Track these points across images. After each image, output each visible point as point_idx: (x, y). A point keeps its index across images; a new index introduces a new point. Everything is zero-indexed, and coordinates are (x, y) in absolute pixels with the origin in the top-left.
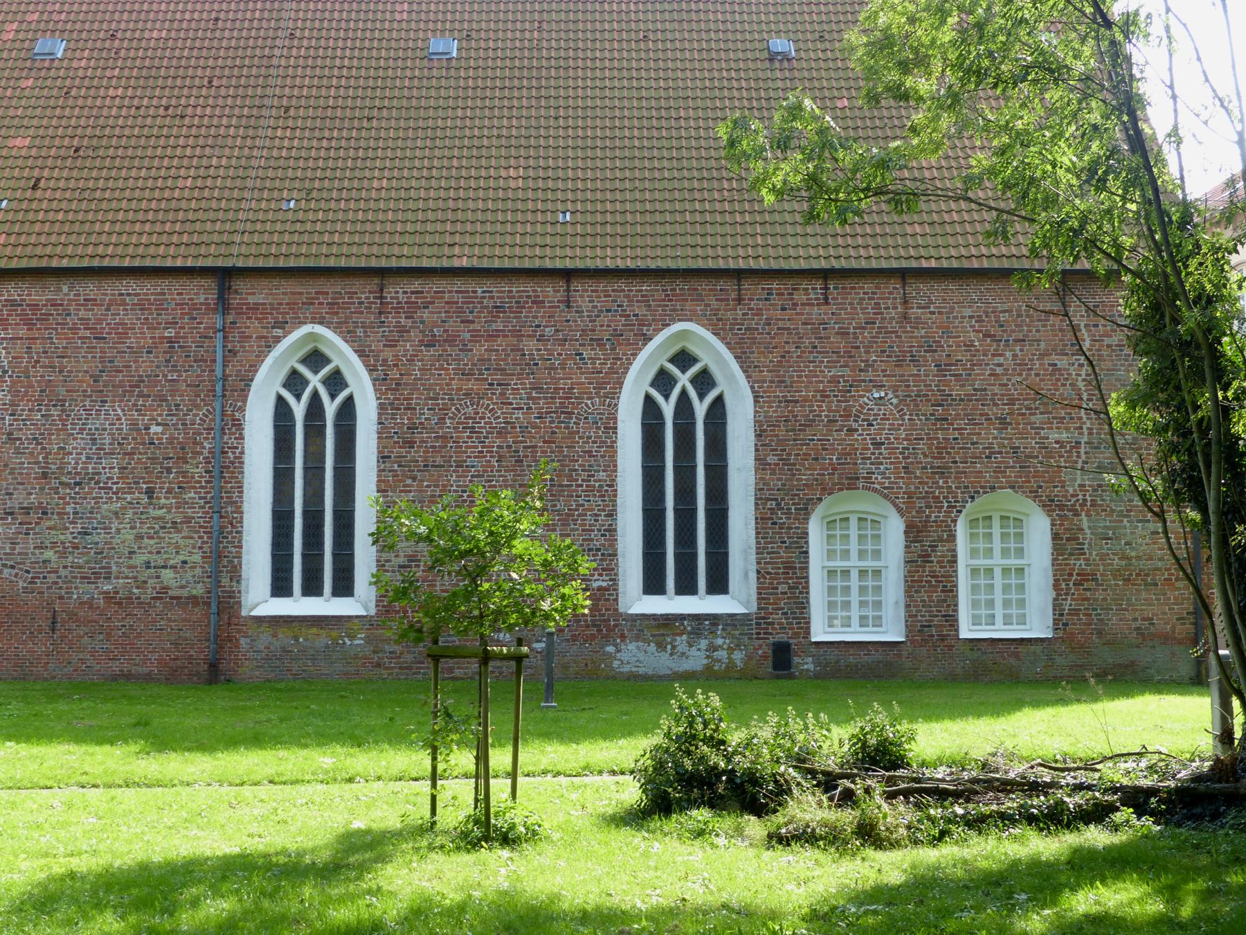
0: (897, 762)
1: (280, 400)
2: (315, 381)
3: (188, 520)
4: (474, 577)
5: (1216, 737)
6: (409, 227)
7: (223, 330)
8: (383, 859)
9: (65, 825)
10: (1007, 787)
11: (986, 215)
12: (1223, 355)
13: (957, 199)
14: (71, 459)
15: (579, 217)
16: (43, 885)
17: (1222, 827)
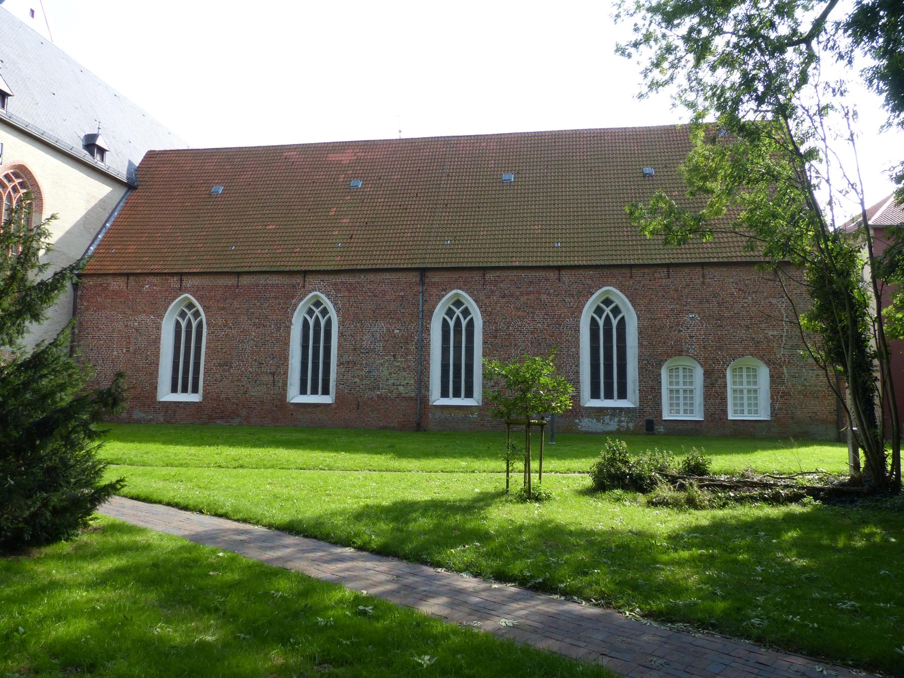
0: (703, 472)
1: (444, 319)
2: (458, 312)
3: (409, 367)
4: (525, 392)
5: (851, 466)
6: (495, 250)
8: (489, 505)
9: (364, 486)
10: (753, 485)
11: (743, 238)
12: (854, 297)
13: (731, 232)
14: (364, 343)
15: (564, 244)
17: (856, 506)
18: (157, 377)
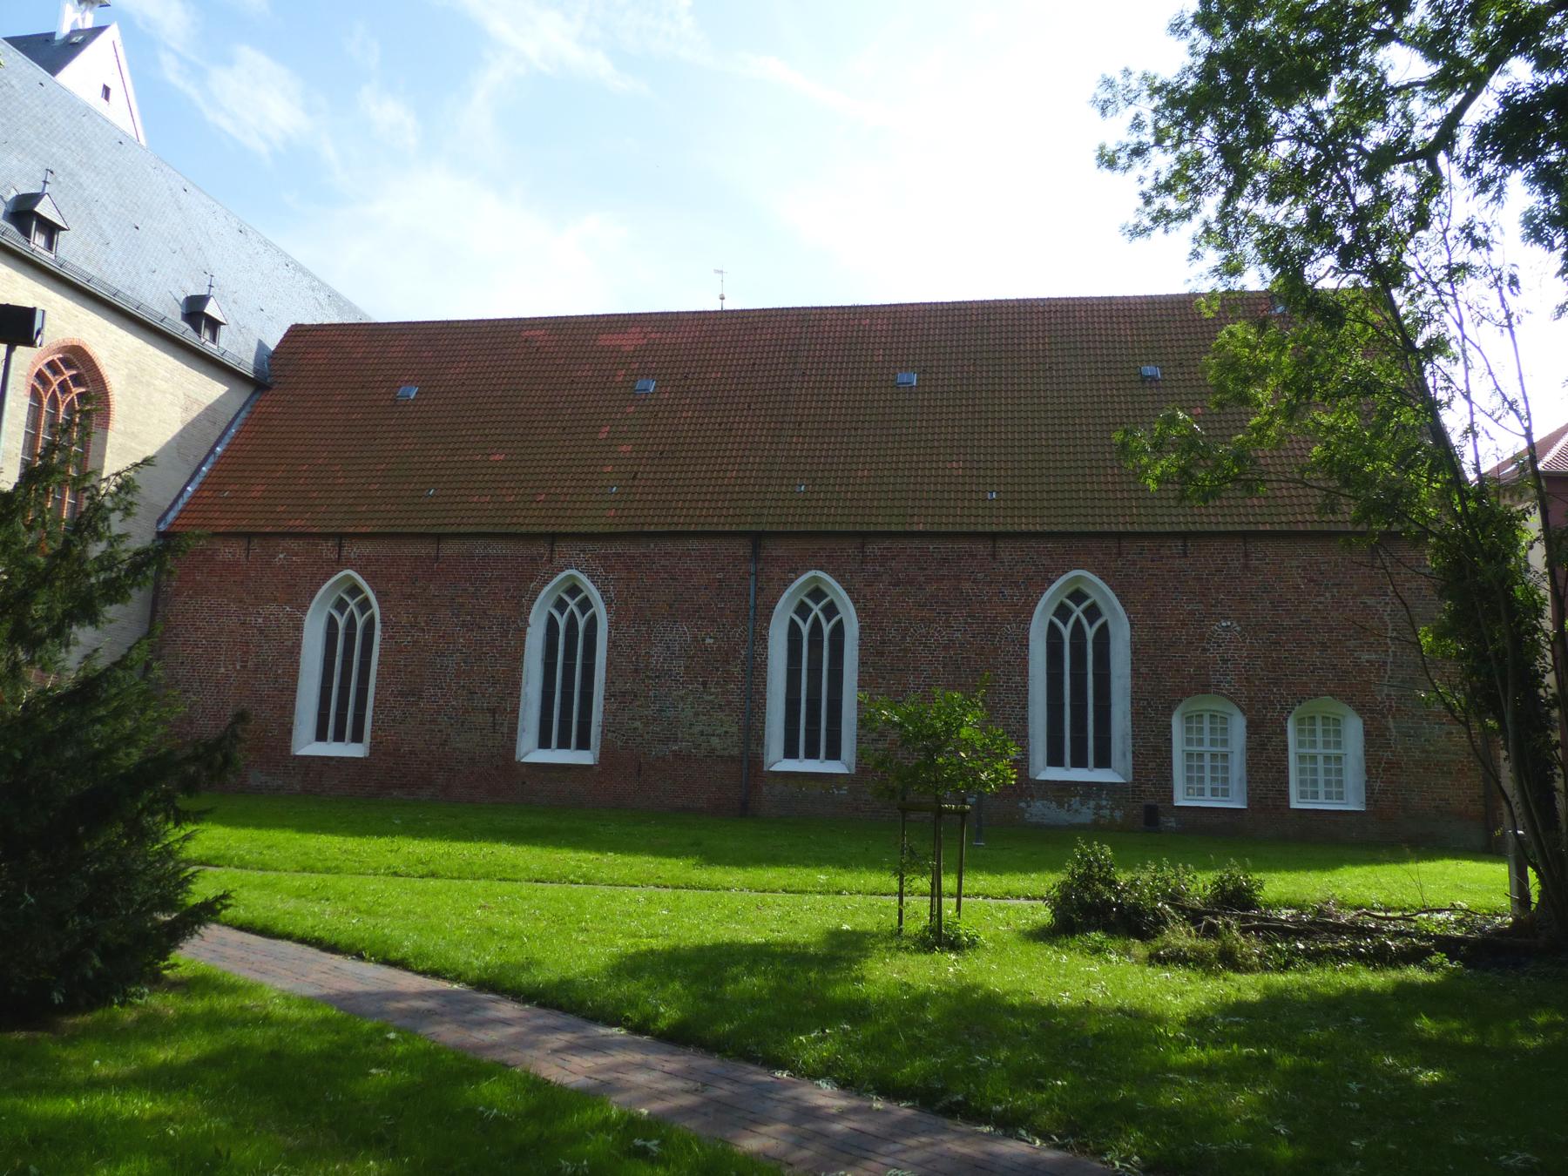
1: (792, 622)
3: (729, 703)
4: (930, 753)
6: (882, 503)
7: (756, 574)
9: (647, 915)
10: (1339, 930)
14: (653, 660)
16: (632, 957)
18: (292, 713)
